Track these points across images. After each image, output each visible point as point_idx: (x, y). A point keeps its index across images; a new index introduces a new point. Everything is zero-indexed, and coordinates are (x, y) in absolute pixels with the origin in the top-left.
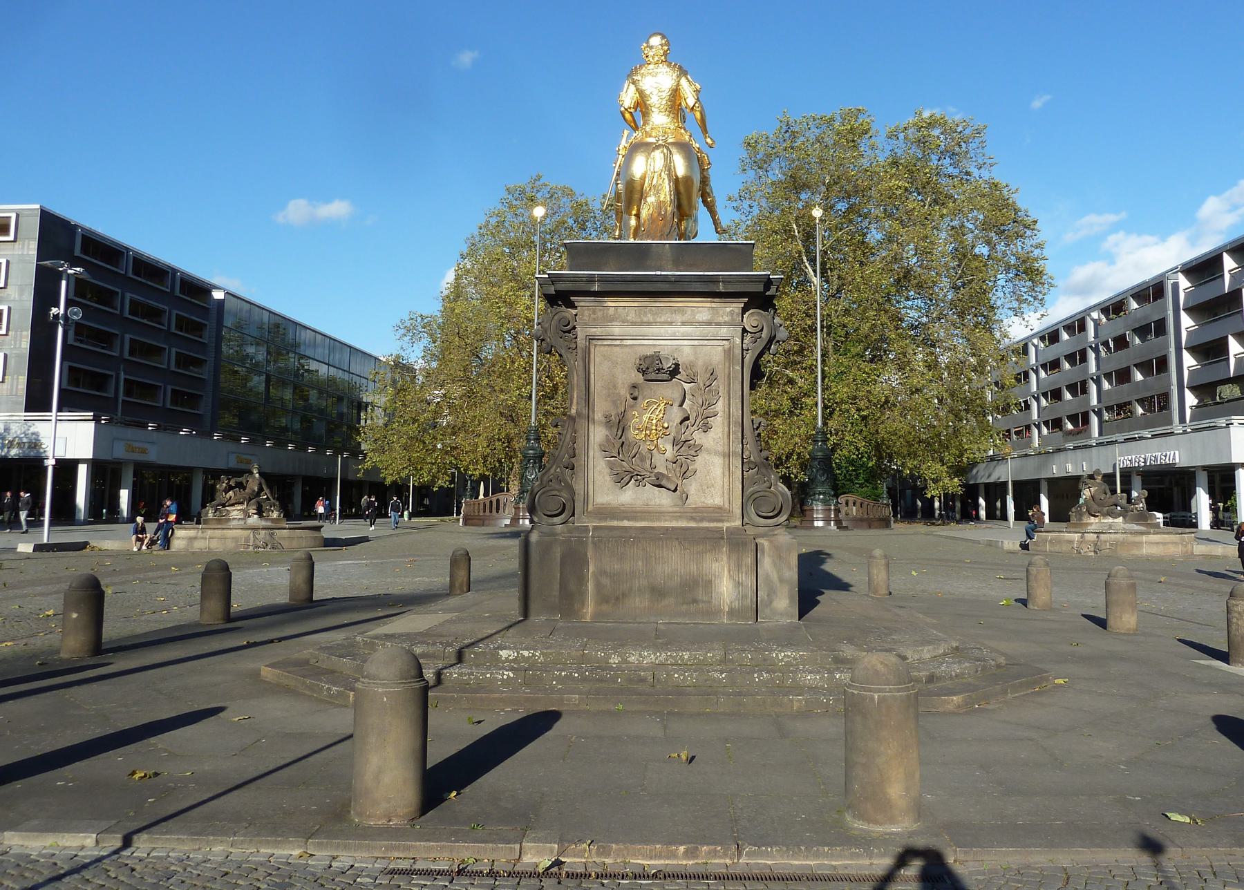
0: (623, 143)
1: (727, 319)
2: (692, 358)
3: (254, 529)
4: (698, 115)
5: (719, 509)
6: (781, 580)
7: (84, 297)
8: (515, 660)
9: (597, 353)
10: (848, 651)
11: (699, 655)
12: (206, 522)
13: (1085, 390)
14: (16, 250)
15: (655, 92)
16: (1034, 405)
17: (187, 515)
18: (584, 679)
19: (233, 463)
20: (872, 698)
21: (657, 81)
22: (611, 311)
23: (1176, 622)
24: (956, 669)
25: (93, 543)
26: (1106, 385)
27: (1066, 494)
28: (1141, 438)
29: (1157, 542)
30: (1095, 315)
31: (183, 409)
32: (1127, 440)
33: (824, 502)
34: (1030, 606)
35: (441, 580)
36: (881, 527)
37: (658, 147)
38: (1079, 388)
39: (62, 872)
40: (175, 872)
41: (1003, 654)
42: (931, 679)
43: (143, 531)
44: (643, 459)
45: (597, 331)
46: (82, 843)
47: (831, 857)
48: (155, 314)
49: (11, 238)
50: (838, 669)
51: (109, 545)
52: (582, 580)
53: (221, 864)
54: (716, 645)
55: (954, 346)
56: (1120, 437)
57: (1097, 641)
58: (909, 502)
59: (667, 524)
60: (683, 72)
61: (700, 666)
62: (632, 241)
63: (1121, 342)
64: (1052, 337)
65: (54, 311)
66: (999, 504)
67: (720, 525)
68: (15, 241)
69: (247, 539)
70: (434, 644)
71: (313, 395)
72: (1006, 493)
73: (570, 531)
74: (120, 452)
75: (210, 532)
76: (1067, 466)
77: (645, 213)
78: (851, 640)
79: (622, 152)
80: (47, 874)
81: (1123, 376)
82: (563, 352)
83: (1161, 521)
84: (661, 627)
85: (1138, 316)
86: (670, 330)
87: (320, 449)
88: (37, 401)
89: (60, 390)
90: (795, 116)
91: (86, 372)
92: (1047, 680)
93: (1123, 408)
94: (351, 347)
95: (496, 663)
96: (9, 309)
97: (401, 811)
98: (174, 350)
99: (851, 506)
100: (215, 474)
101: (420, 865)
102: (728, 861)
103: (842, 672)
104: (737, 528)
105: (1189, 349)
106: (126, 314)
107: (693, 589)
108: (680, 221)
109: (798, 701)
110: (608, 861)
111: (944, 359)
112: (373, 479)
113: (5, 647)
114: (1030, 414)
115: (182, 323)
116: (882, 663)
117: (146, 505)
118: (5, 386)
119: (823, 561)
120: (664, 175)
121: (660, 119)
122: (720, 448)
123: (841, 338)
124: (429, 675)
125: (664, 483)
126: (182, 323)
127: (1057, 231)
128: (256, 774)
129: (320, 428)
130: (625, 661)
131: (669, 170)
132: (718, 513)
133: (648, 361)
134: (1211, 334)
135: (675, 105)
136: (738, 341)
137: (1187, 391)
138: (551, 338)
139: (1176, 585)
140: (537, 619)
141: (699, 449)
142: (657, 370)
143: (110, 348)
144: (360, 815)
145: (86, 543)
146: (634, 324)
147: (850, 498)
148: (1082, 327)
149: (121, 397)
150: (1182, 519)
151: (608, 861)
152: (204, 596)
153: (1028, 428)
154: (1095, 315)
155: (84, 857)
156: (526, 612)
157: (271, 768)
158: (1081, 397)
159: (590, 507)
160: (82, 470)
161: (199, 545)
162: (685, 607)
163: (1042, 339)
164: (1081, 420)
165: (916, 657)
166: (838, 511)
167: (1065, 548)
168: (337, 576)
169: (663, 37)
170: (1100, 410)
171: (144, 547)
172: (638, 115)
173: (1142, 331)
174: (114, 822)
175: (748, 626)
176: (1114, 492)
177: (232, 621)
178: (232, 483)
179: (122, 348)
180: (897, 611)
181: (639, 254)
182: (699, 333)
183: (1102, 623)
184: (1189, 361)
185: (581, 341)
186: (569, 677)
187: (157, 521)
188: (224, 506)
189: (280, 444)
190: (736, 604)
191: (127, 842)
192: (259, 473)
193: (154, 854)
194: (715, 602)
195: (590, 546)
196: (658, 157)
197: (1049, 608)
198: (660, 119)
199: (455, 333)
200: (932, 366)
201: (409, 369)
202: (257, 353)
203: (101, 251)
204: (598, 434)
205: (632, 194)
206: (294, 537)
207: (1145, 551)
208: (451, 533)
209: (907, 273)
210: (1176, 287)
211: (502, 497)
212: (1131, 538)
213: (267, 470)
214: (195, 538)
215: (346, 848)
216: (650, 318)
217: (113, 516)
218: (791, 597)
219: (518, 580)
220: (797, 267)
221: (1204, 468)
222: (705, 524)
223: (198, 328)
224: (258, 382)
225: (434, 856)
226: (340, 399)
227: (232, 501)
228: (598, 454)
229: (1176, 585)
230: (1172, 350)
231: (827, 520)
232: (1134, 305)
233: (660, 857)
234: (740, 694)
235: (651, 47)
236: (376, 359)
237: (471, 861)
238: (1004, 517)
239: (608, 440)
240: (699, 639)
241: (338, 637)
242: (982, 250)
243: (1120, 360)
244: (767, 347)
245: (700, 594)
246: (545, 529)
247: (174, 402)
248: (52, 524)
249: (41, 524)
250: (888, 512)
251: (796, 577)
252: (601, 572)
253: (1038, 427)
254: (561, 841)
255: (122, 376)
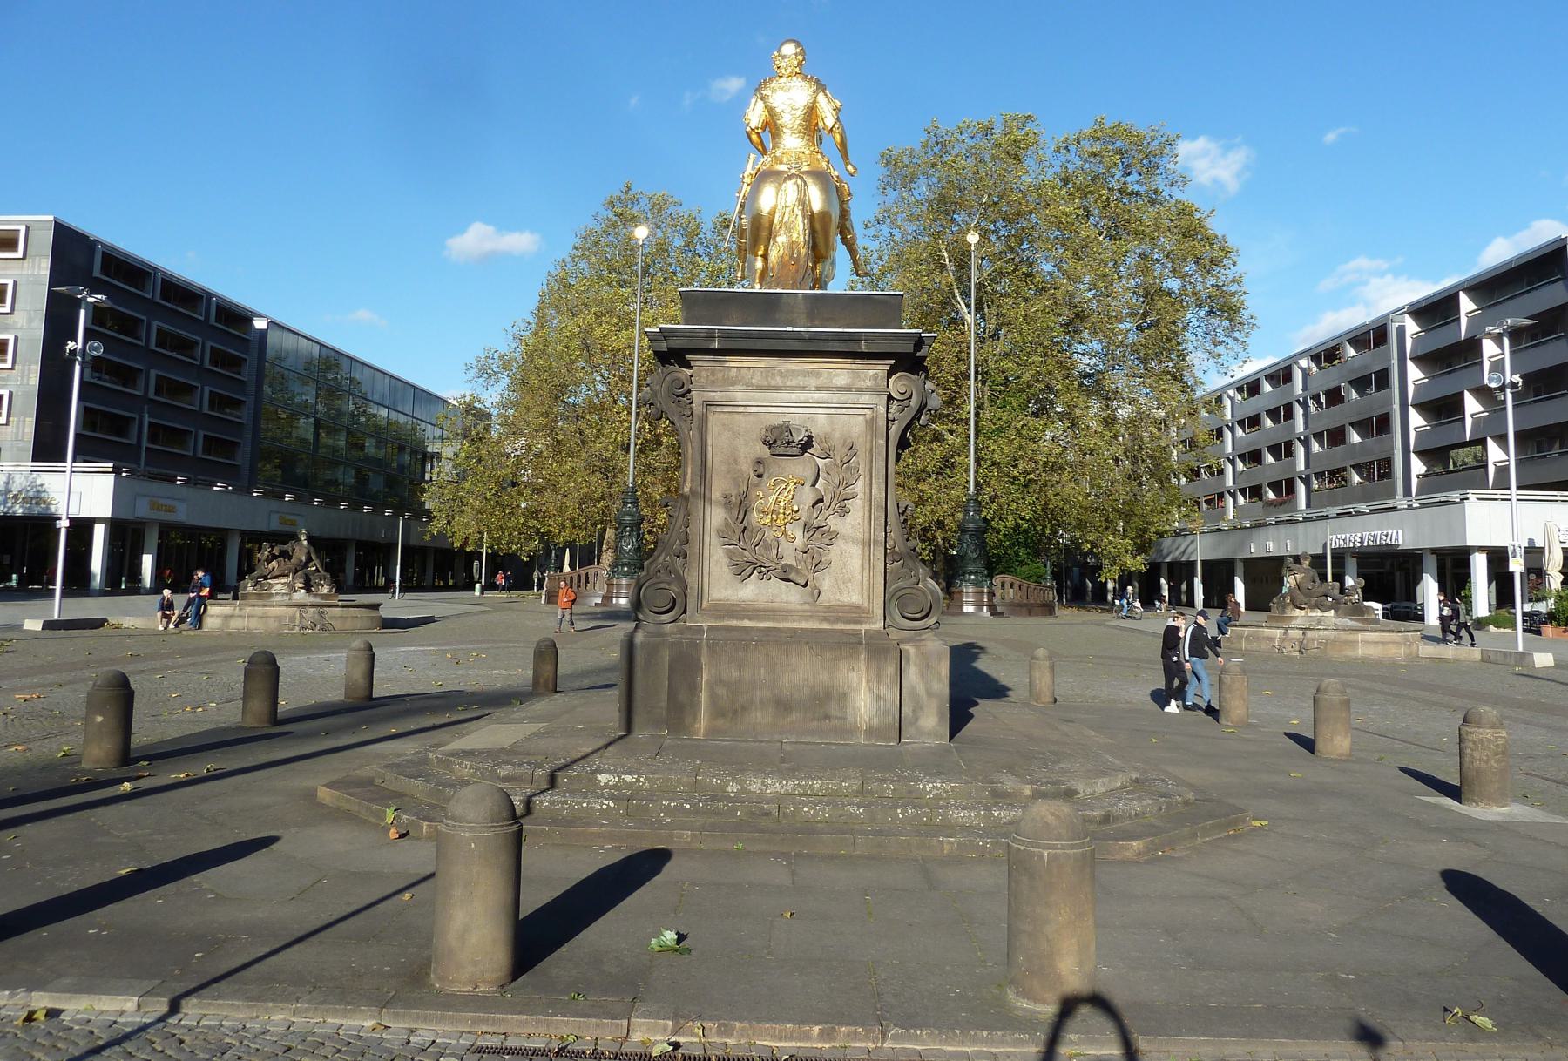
0: (749, 170)
1: (869, 383)
2: (828, 429)
3: (301, 606)
4: (838, 137)
5: (857, 608)
6: (929, 694)
7: (102, 325)
8: (616, 786)
9: (716, 421)
10: (1008, 783)
11: (832, 784)
12: (245, 597)
13: (1290, 453)
14: (26, 269)
15: (788, 110)
16: (1229, 468)
17: (220, 587)
18: (696, 811)
19: (275, 525)
20: (1041, 856)
21: (791, 97)
22: (734, 372)
23: (1397, 745)
24: (1137, 807)
25: (112, 620)
26: (1316, 447)
27: (1266, 578)
28: (1359, 513)
29: (1376, 641)
30: (1304, 363)
31: (217, 459)
32: (1340, 515)
33: (976, 583)
34: (1223, 721)
35: (520, 673)
36: (1044, 615)
37: (790, 177)
38: (1283, 450)
39: (101, 1043)
40: (230, 1046)
41: (1191, 786)
42: (1106, 819)
43: (170, 606)
44: (768, 548)
45: (716, 396)
46: (121, 1007)
47: (991, 1042)
48: (185, 346)
49: (20, 254)
50: (996, 805)
51: (129, 622)
52: (694, 689)
53: (284, 1036)
54: (851, 772)
55: (1136, 398)
56: (1331, 511)
57: (1301, 770)
58: (1079, 583)
59: (795, 625)
60: (821, 87)
61: (832, 798)
62: (757, 288)
63: (1335, 396)
64: (1251, 388)
65: (71, 345)
66: (1184, 587)
67: (857, 627)
68: (24, 258)
69: (293, 618)
70: (520, 765)
71: (370, 447)
72: (1192, 575)
73: (681, 631)
74: (143, 511)
75: (248, 609)
76: (1269, 544)
77: (774, 255)
78: (1011, 770)
79: (748, 180)
80: (84, 1045)
81: (1336, 437)
82: (676, 420)
83: (1380, 612)
84: (788, 748)
85: (1357, 365)
86: (802, 396)
87: (378, 509)
88: (47, 448)
89: (77, 435)
90: (947, 126)
91: (105, 414)
92: (1244, 820)
93: (1336, 475)
94: (414, 387)
95: (594, 790)
96: (16, 338)
97: (488, 976)
98: (207, 389)
99: (1007, 587)
100: (257, 538)
101: (511, 1043)
102: (871, 1045)
103: (1001, 808)
104: (878, 631)
105: (1416, 406)
106: (153, 346)
107: (825, 703)
108: (815, 263)
109: (949, 844)
110: (730, 1041)
111: (1124, 413)
112: (438, 545)
113: (16, 754)
114: (1223, 481)
115: (218, 358)
116: (1053, 814)
117: (173, 574)
118: (9, 429)
119: (975, 657)
120: (798, 211)
121: (792, 142)
122: (859, 536)
123: (999, 388)
124: (519, 806)
125: (792, 576)
126: (218, 358)
127: (1256, 270)
128: (319, 924)
129: (377, 484)
130: (744, 790)
131: (804, 204)
132: (856, 613)
133: (776, 433)
134: (1444, 388)
135: (810, 125)
136: (883, 410)
137: (1409, 363)
138: (663, 402)
139: (1397, 696)
140: (641, 734)
141: (835, 535)
142: (787, 443)
143: (134, 386)
144: (441, 979)
145: (105, 620)
146: (760, 388)
147: (1007, 578)
148: (1288, 377)
149: (145, 444)
150: (1405, 610)
151: (730, 1041)
152: (246, 697)
153: (1221, 496)
154: (1304, 363)
155: (125, 1024)
156: (629, 727)
157: (335, 917)
158: (1285, 460)
159: (705, 603)
160: (99, 532)
161: (236, 624)
162: (815, 723)
163: (1240, 390)
164: (1285, 488)
165: (1089, 791)
166: (992, 594)
167: (1264, 646)
168: (405, 667)
169: (798, 44)
170: (1308, 477)
171: (171, 626)
172: (767, 137)
173: (1361, 383)
174: (157, 982)
175: (887, 753)
176: (1323, 577)
177: (278, 725)
178: (276, 551)
179: (146, 386)
180: (1064, 727)
181: (767, 306)
182: (836, 400)
183: (1308, 745)
184: (1416, 420)
185: (697, 407)
186: (679, 809)
187: (187, 592)
188: (266, 578)
189: (331, 502)
190: (876, 721)
191: (174, 1007)
192: (309, 539)
193: (204, 1022)
194: (851, 719)
195: (704, 650)
196: (791, 187)
197: (1244, 725)
198: (792, 142)
199: (541, 373)
200: (1109, 422)
201: (484, 415)
202: (308, 395)
203: (124, 272)
204: (716, 517)
205: (759, 231)
206: (346, 614)
207: (1361, 651)
208: (530, 615)
209: (1081, 316)
210: (1401, 331)
211: (591, 570)
212: (1343, 636)
213: (316, 533)
214: (232, 616)
215: (426, 1019)
216: (779, 381)
217: (135, 588)
218: (941, 714)
219: (620, 679)
220: (948, 302)
221: (1434, 551)
222: (840, 626)
223: (235, 363)
224: (305, 427)
225: (527, 1031)
226: (401, 449)
227: (276, 573)
228: (715, 540)
229: (1397, 696)
230: (1396, 407)
231: (979, 605)
232: (1351, 352)
233: (791, 1038)
234: (880, 833)
235: (784, 57)
236: (445, 401)
237: (571, 1038)
238: (1191, 603)
239: (727, 525)
240: (831, 764)
241: (408, 747)
242: (1173, 284)
243: (1330, 418)
244: (917, 416)
245: (833, 709)
246: (652, 628)
247: (207, 450)
248: (64, 594)
249: (51, 594)
250: (1052, 596)
251: (946, 691)
252: (717, 681)
253: (1233, 495)
254: (676, 1016)
255: (147, 419)
